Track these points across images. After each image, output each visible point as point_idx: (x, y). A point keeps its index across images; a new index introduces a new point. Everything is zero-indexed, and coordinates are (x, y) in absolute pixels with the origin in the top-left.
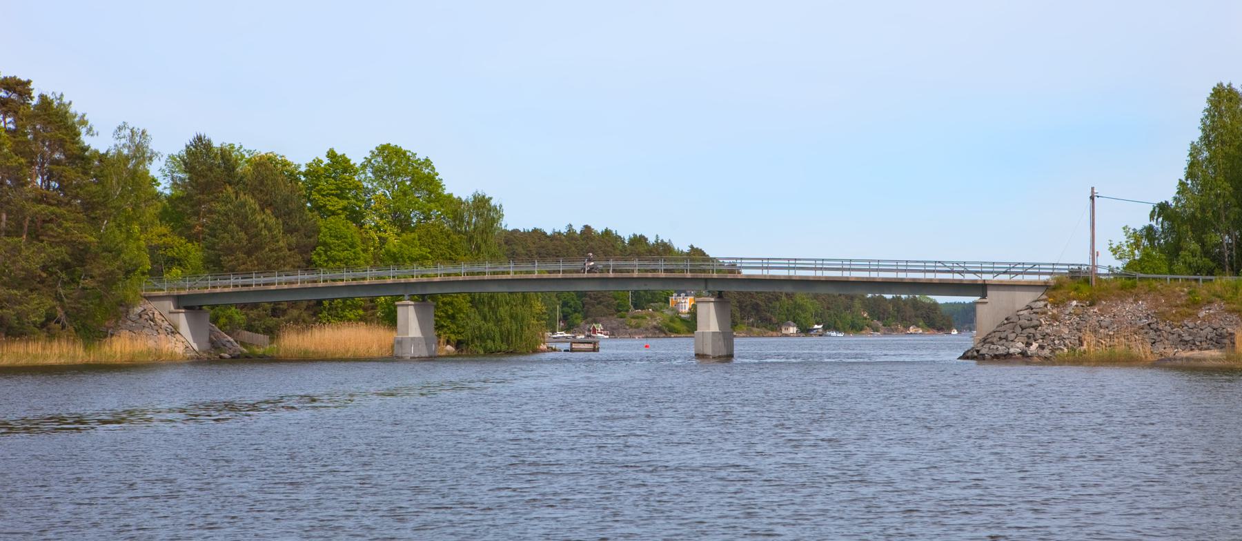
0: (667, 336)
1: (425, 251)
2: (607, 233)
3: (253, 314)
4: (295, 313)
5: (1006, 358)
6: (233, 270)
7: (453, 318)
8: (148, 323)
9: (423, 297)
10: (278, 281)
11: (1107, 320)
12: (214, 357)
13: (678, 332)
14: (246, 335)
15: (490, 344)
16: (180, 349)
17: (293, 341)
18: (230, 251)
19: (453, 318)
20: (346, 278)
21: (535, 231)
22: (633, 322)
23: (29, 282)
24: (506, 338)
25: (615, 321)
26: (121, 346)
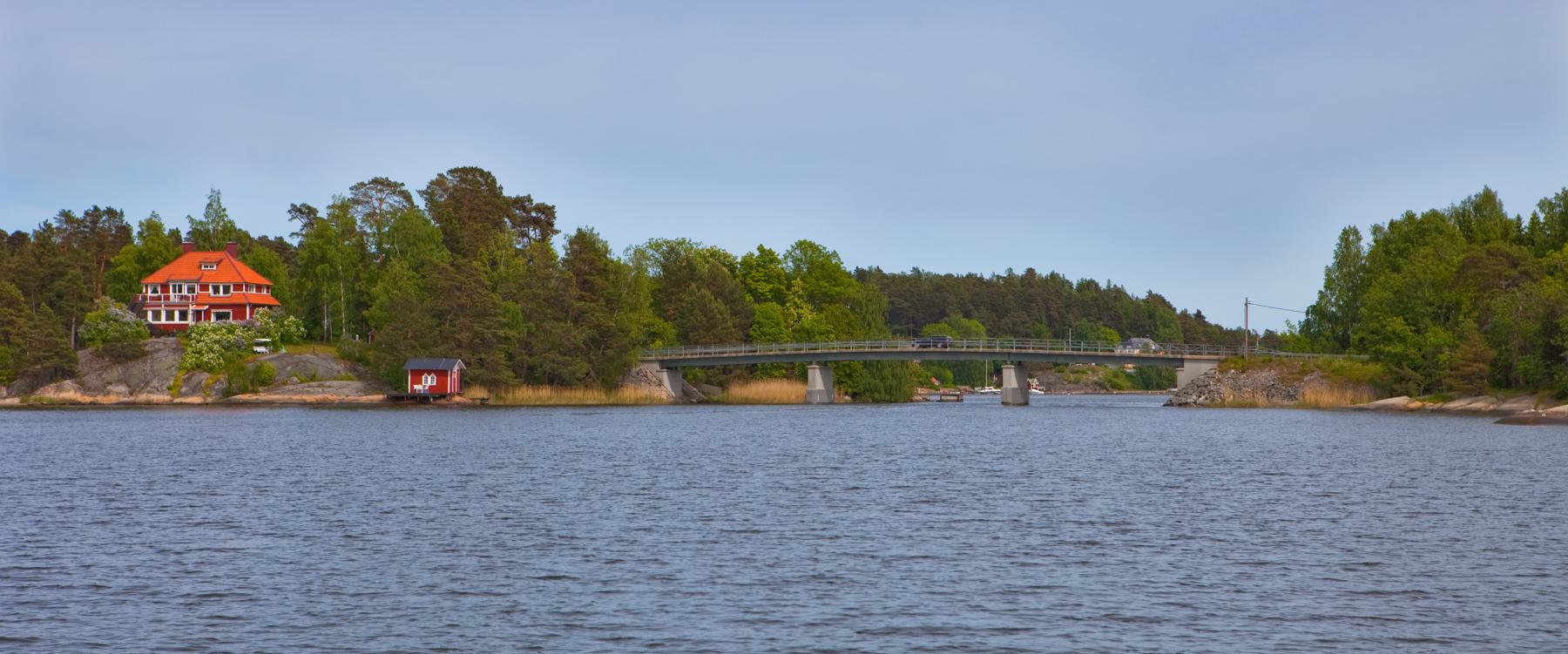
0: (1108, 392)
1: (830, 327)
2: (1053, 276)
3: (710, 372)
4: (738, 371)
5: (1186, 404)
6: (696, 343)
7: (850, 376)
8: (643, 378)
9: (825, 364)
10: (729, 351)
11: (1249, 381)
12: (685, 400)
13: (1121, 388)
14: (706, 387)
15: (876, 395)
16: (664, 396)
17: (737, 391)
18: (695, 329)
19: (850, 376)
20: (775, 349)
21: (970, 276)
22: (1072, 377)
23: (574, 351)
24: (889, 391)
25: (1052, 376)
26: (629, 393)
